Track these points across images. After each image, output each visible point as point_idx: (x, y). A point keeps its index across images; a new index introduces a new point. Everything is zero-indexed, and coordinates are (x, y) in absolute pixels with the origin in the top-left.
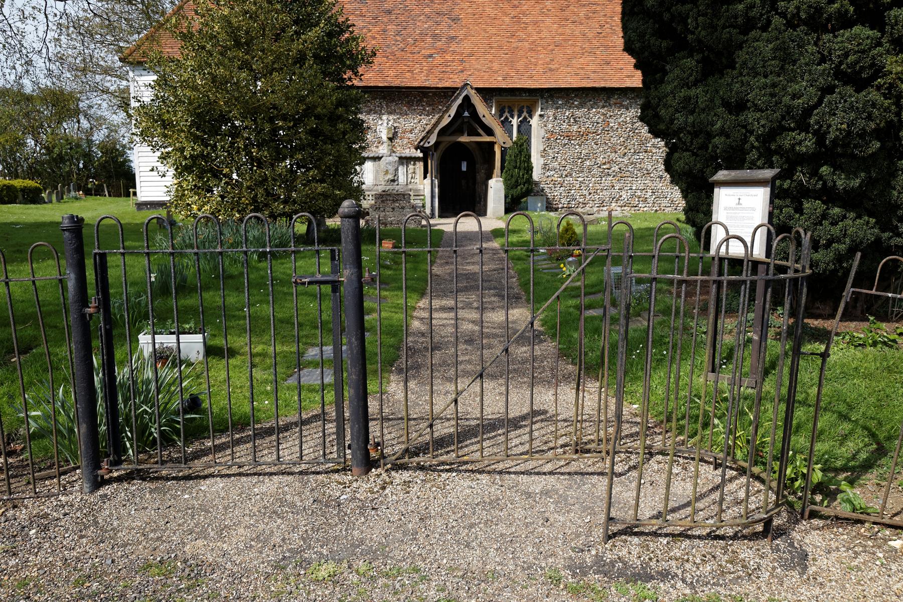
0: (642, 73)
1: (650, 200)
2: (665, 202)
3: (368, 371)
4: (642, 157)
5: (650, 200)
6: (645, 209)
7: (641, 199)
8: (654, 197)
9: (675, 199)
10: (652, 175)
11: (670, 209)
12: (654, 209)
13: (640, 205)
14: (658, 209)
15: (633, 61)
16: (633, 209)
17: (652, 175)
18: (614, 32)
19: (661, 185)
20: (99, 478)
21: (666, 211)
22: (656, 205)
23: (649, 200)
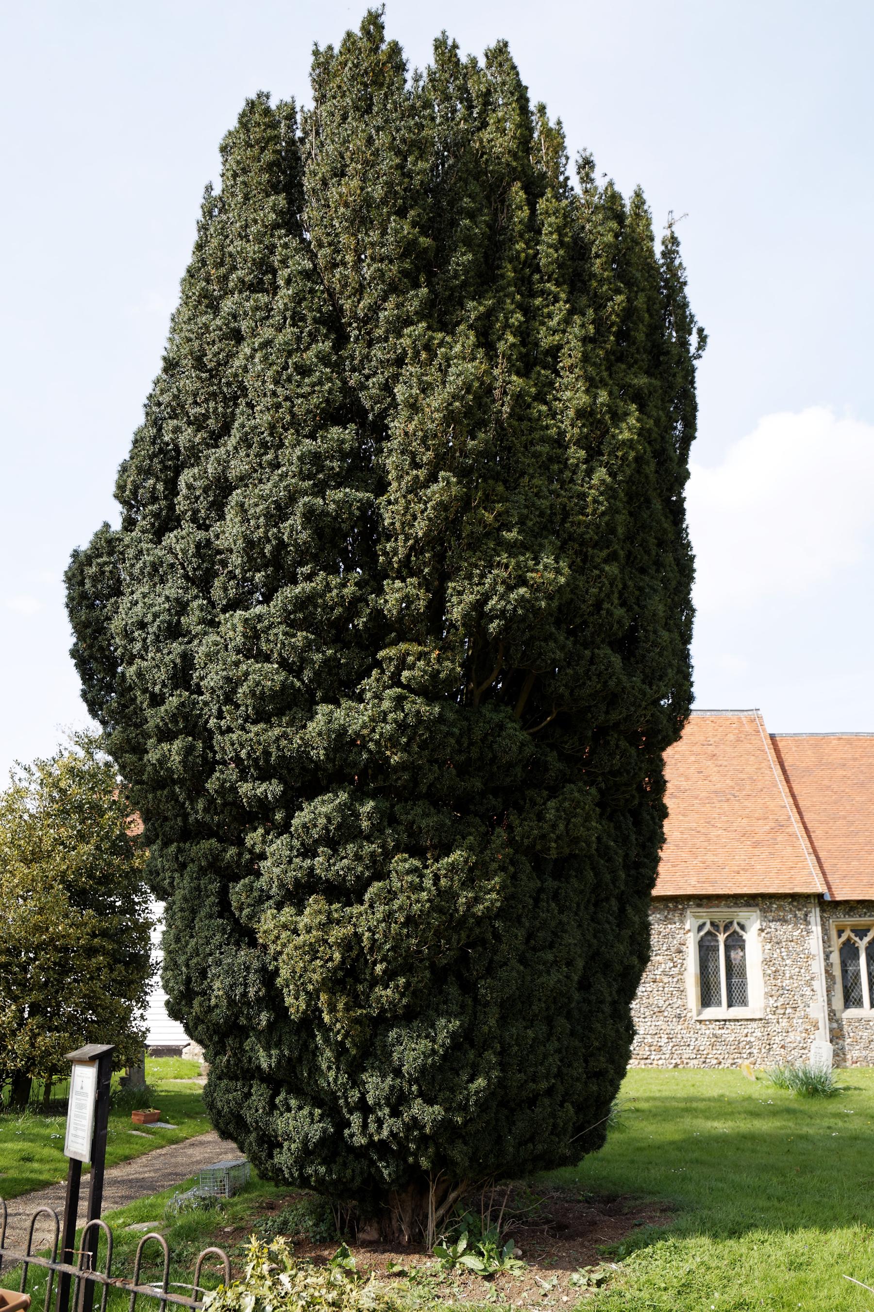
0: (664, 749)
1: (667, 1050)
2: (687, 1053)
3: (105, 1182)
4: (649, 989)
5: (667, 1050)
6: (660, 1062)
7: (653, 1048)
8: (671, 1044)
9: (702, 1048)
10: (666, 1014)
11: (695, 1062)
12: (674, 1061)
13: (652, 1057)
14: (679, 1061)
15: (692, 690)
16: (643, 1062)
17: (666, 1014)
18: (85, 1118)
19: (680, 1027)
20: (561, 178)
21: (691, 1064)
22: (675, 1056)
23: (664, 1049)
